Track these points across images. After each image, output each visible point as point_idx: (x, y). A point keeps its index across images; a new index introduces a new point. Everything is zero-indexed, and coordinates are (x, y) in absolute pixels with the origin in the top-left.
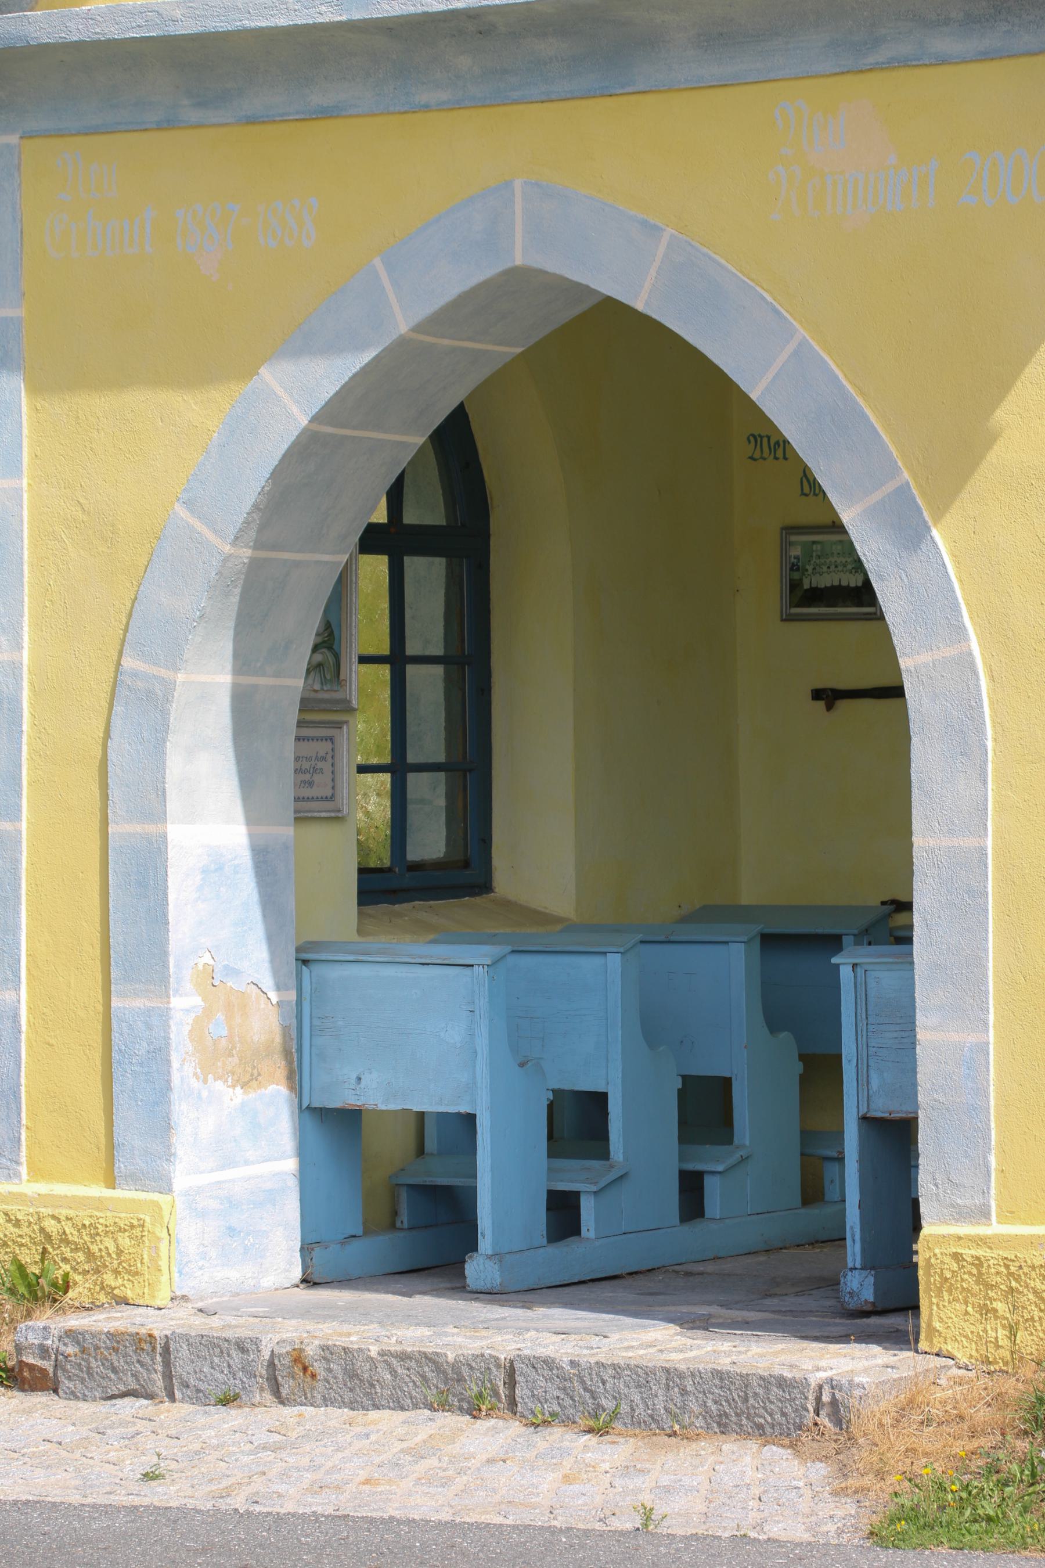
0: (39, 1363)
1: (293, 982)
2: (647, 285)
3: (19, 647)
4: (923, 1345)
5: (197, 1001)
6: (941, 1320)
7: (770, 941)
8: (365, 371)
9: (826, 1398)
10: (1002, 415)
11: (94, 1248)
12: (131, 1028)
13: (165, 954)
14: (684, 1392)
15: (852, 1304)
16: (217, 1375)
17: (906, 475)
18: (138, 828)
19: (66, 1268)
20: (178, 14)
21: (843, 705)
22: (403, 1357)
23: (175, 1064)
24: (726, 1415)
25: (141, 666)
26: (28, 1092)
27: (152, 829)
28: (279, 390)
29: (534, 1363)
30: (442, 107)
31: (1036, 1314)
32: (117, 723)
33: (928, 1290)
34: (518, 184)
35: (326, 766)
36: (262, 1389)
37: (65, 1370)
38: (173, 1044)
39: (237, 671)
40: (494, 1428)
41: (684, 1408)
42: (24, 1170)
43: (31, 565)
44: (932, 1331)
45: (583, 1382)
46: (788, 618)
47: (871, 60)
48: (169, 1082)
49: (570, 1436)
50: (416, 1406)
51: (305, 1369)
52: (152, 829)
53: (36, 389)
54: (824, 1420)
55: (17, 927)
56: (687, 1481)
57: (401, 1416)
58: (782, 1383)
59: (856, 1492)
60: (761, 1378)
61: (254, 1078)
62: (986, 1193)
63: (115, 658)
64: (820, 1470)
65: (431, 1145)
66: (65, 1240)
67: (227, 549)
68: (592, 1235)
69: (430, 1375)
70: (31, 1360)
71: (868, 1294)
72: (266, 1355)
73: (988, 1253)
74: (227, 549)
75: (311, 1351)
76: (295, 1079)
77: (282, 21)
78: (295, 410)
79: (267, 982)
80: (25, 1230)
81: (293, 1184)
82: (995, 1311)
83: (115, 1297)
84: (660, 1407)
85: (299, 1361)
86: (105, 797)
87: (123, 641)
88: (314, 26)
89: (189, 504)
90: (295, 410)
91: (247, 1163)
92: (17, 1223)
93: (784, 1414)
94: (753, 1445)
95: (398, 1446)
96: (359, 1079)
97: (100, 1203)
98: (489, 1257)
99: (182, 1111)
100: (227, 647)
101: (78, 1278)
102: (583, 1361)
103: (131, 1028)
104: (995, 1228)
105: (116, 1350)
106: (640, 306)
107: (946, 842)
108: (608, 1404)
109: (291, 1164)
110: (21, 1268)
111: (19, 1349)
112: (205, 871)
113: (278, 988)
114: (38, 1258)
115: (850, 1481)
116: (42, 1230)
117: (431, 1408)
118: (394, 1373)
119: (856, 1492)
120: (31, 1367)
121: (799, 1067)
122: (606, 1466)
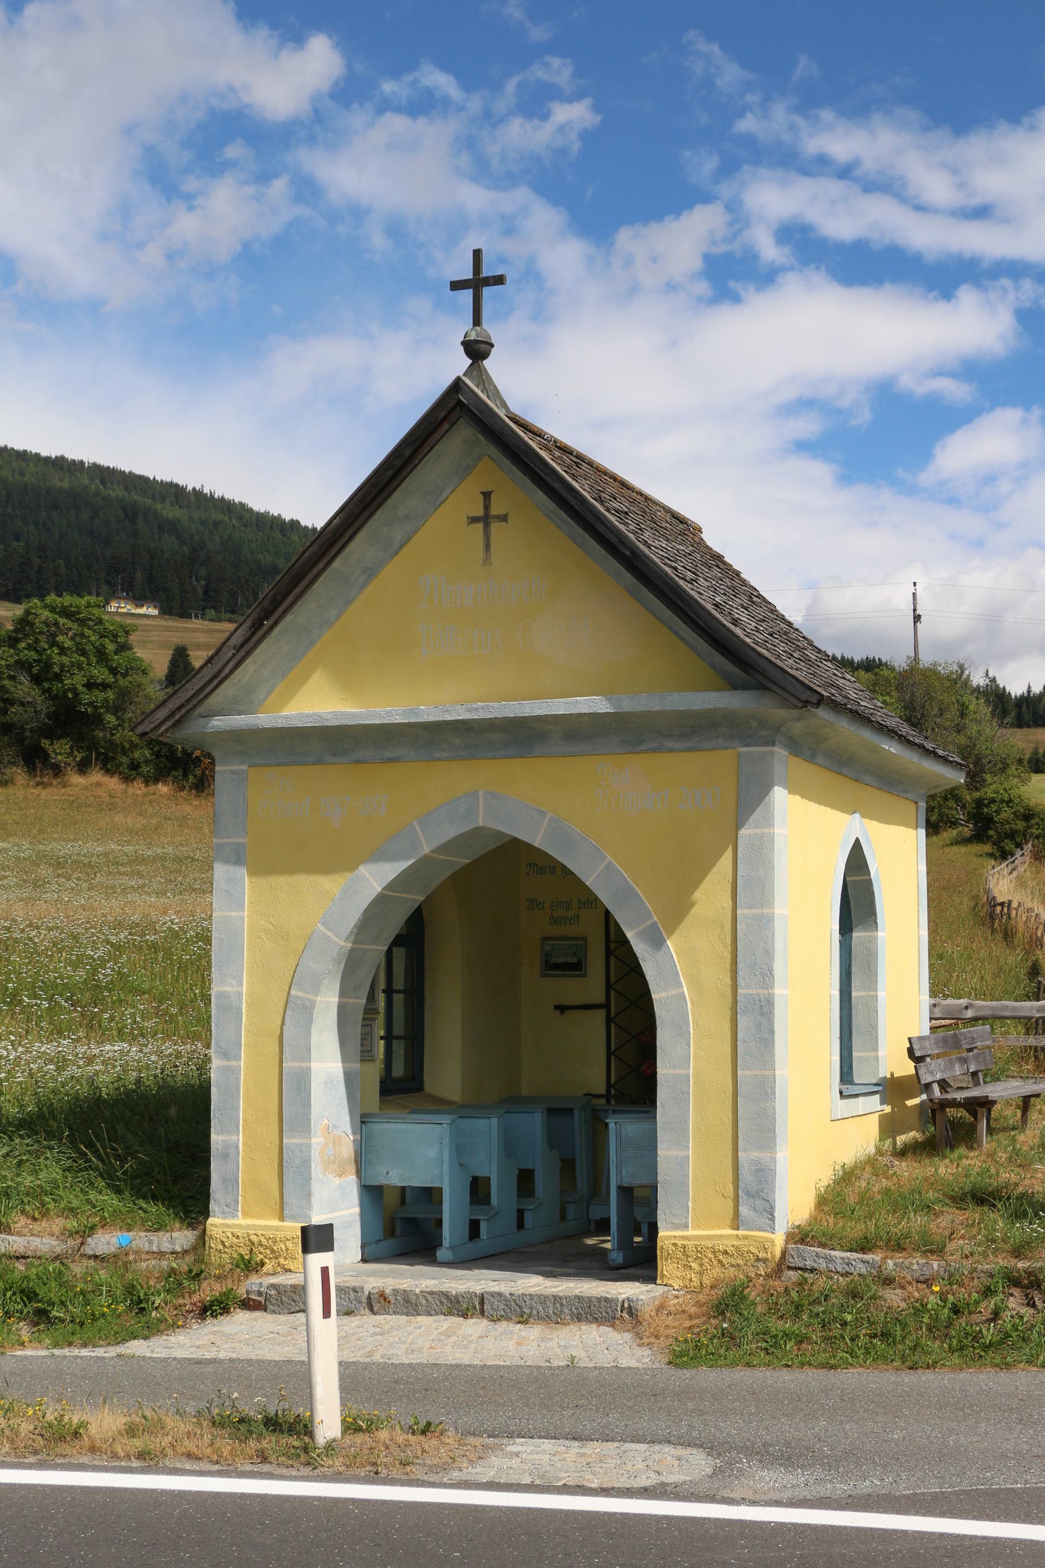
0: (258, 1298)
1: (359, 1131)
2: (540, 836)
3: (242, 985)
4: (659, 1281)
5: (322, 1140)
6: (667, 1271)
7: (551, 1112)
8: (408, 868)
9: (626, 1305)
10: (697, 895)
11: (275, 1248)
12: (292, 1152)
13: (310, 1119)
14: (562, 1305)
15: (613, 1265)
16: (343, 1303)
17: (655, 918)
18: (297, 1065)
19: (262, 1257)
20: (329, 717)
21: (568, 1012)
22: (431, 1293)
23: (313, 1167)
24: (581, 1314)
25: (300, 994)
26: (242, 1180)
27: (304, 1065)
28: (368, 876)
29: (493, 1294)
30: (446, 759)
31: (708, 1267)
32: (287, 1018)
33: (661, 1259)
34: (481, 793)
35: (369, 1038)
36: (364, 1308)
37: (270, 1301)
38: (312, 1158)
39: (340, 997)
40: (476, 1323)
41: (562, 1312)
42: (240, 1214)
43: (248, 949)
44: (663, 1275)
45: (516, 1302)
46: (544, 976)
47: (640, 748)
48: (310, 1175)
49: (511, 1325)
50: (437, 1314)
51: (385, 1299)
52: (304, 1065)
53: (252, 873)
54: (625, 1315)
55: (239, 1108)
56: (571, 1343)
57: (431, 1319)
58: (606, 1300)
59: (648, 1344)
60: (597, 1298)
61: (343, 1173)
62: (687, 1218)
63: (287, 990)
64: (627, 1336)
65: (408, 1199)
66: (260, 1244)
67: (342, 943)
68: (485, 1237)
69: (444, 1300)
70: (254, 1297)
71: (620, 1260)
72: (367, 1293)
73: (688, 1243)
74: (342, 943)
75: (387, 1292)
76: (359, 1173)
77: (378, 722)
78: (375, 884)
79: (349, 1131)
80: (242, 1240)
81: (358, 1218)
82: (691, 1266)
83: (284, 1269)
84: (551, 1312)
85: (382, 1295)
86: (281, 1051)
87: (291, 983)
88: (393, 724)
89: (324, 924)
90: (375, 884)
91: (341, 1210)
92: (238, 1237)
93: (607, 1313)
94: (594, 1326)
95: (436, 1332)
96: (388, 1173)
97: (278, 1229)
98: (448, 1248)
99: (316, 1188)
100: (337, 986)
101: (267, 1261)
102: (516, 1293)
103: (292, 1152)
104: (691, 1232)
105: (295, 1292)
106: (536, 845)
107: (672, 1071)
108: (527, 1311)
109: (357, 1210)
110: (242, 1256)
111: (248, 1292)
112: (325, 1083)
113: (354, 1133)
114: (248, 1252)
115: (645, 1340)
116: (250, 1240)
117: (444, 1314)
118: (427, 1300)
119: (648, 1344)
120: (254, 1300)
121: (560, 1164)
122: (533, 1338)
